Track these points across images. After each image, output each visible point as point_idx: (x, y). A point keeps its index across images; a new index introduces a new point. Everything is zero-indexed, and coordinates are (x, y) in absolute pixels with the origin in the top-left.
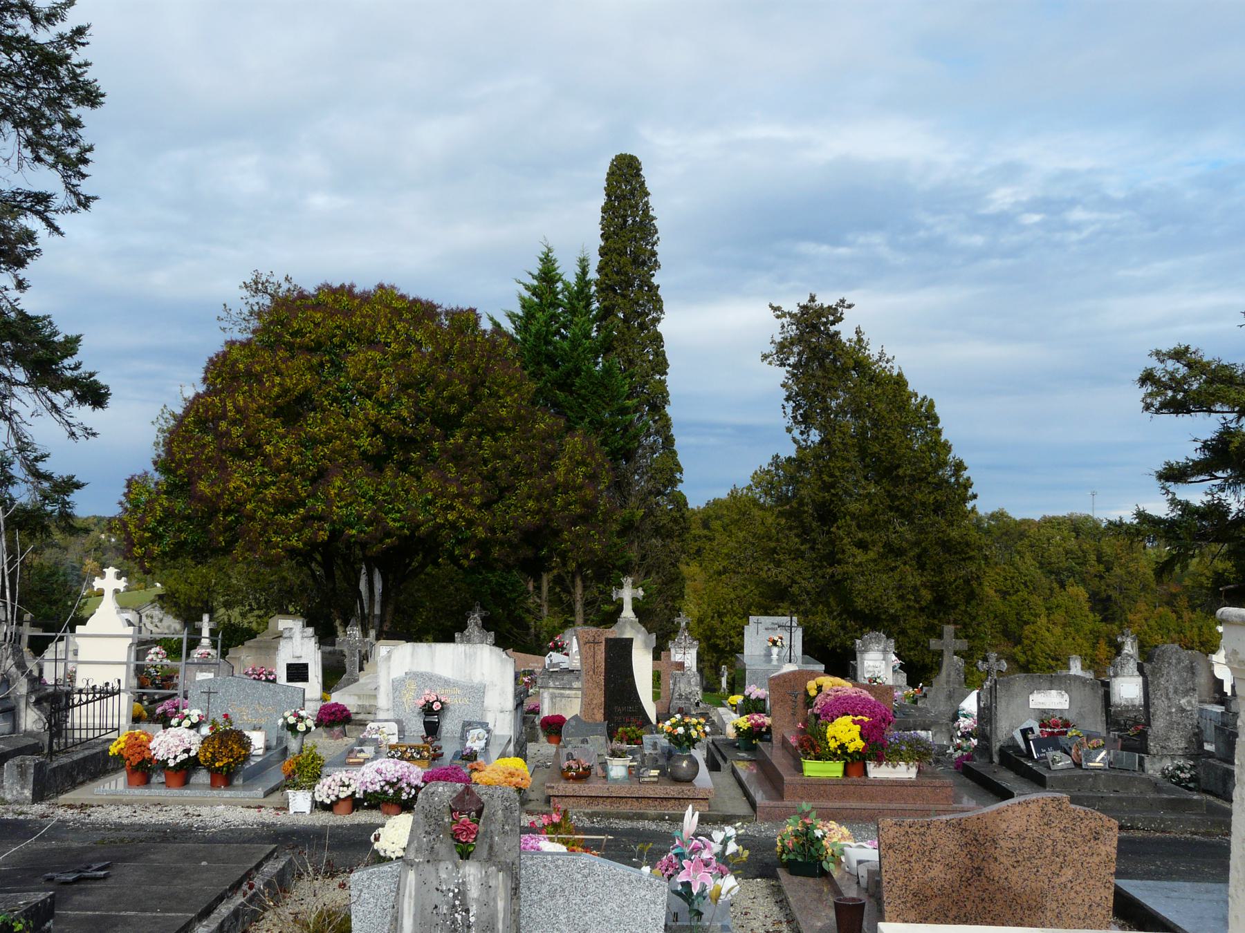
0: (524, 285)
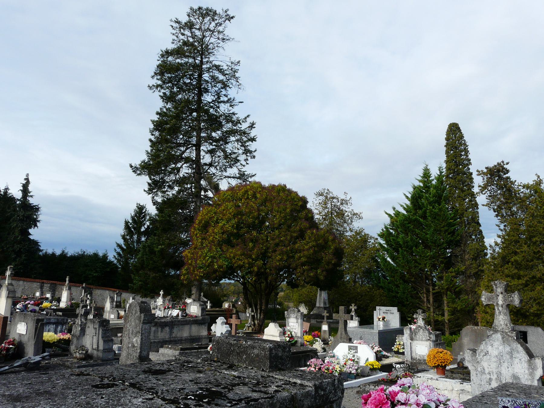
0: (418, 180)
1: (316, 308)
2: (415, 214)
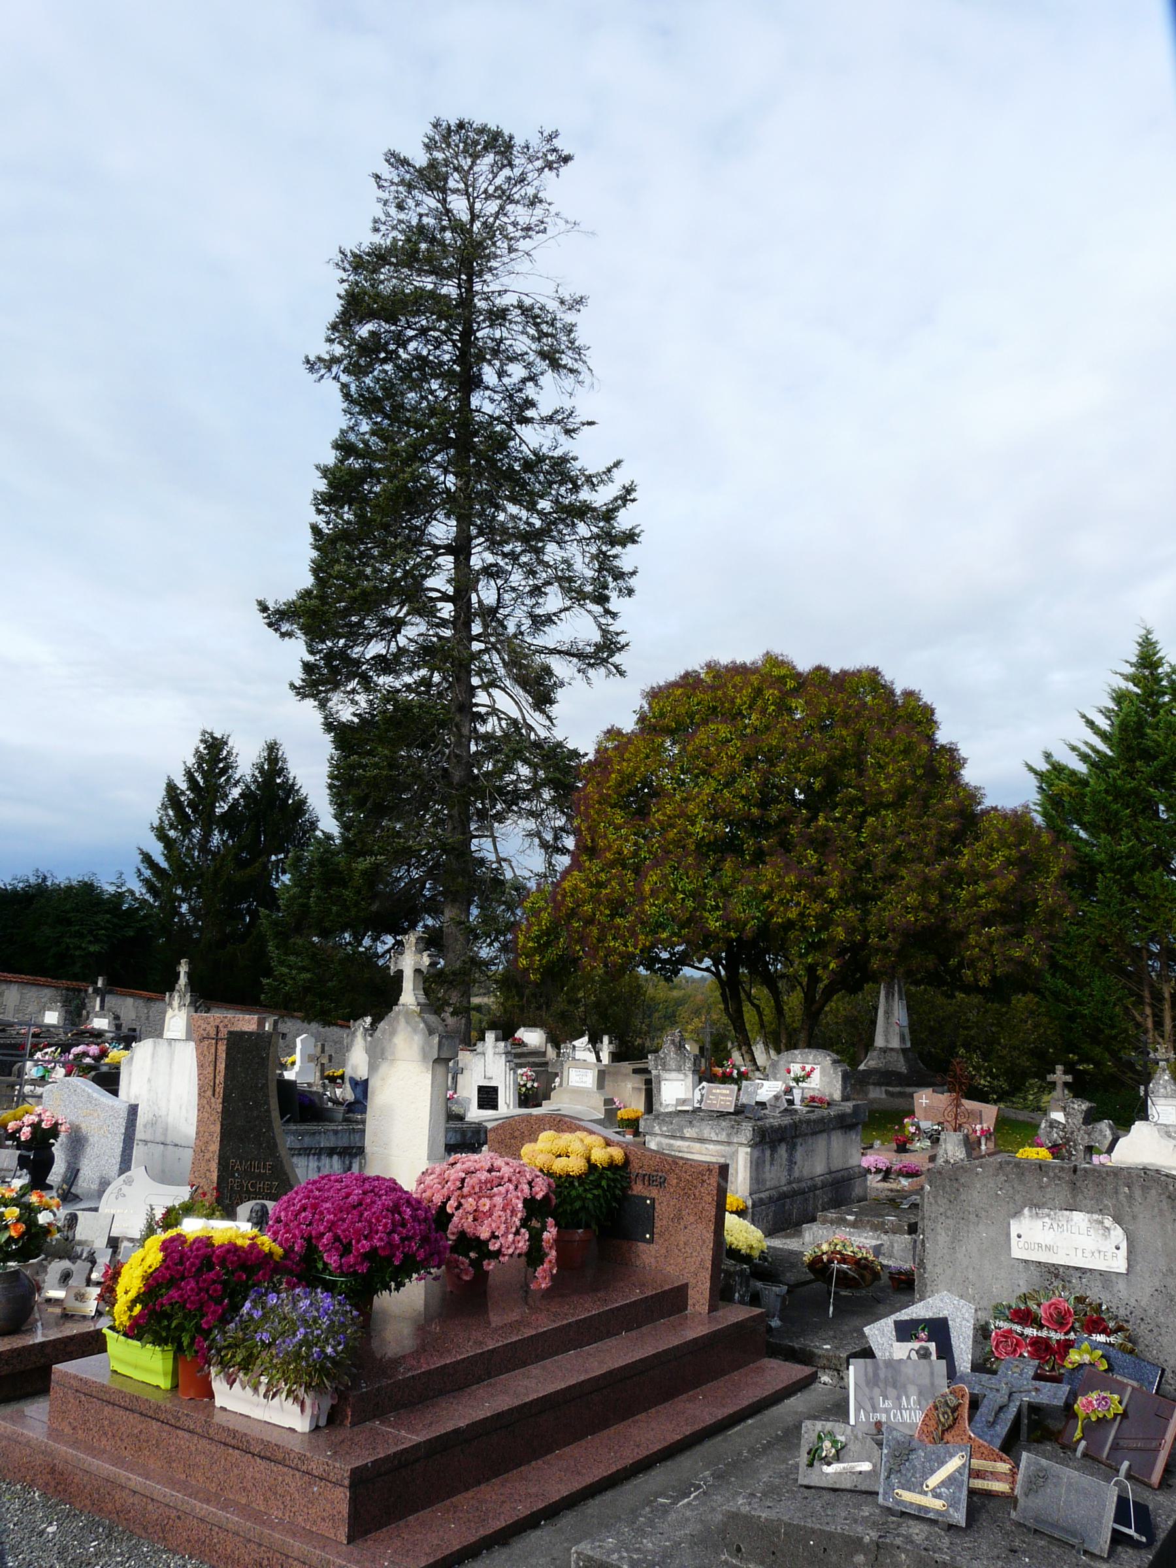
0: (1121, 675)
1: (875, 1053)
2: (1130, 773)
